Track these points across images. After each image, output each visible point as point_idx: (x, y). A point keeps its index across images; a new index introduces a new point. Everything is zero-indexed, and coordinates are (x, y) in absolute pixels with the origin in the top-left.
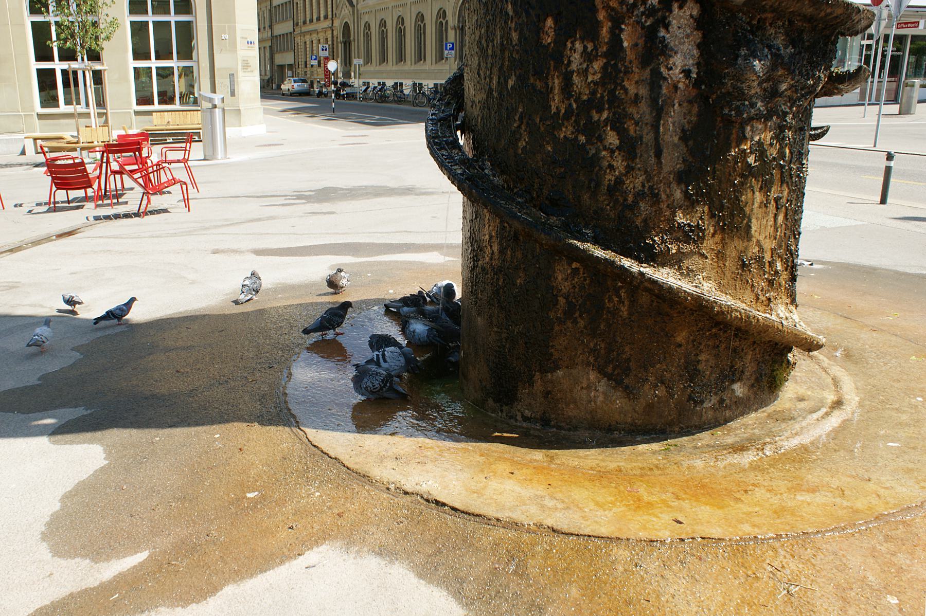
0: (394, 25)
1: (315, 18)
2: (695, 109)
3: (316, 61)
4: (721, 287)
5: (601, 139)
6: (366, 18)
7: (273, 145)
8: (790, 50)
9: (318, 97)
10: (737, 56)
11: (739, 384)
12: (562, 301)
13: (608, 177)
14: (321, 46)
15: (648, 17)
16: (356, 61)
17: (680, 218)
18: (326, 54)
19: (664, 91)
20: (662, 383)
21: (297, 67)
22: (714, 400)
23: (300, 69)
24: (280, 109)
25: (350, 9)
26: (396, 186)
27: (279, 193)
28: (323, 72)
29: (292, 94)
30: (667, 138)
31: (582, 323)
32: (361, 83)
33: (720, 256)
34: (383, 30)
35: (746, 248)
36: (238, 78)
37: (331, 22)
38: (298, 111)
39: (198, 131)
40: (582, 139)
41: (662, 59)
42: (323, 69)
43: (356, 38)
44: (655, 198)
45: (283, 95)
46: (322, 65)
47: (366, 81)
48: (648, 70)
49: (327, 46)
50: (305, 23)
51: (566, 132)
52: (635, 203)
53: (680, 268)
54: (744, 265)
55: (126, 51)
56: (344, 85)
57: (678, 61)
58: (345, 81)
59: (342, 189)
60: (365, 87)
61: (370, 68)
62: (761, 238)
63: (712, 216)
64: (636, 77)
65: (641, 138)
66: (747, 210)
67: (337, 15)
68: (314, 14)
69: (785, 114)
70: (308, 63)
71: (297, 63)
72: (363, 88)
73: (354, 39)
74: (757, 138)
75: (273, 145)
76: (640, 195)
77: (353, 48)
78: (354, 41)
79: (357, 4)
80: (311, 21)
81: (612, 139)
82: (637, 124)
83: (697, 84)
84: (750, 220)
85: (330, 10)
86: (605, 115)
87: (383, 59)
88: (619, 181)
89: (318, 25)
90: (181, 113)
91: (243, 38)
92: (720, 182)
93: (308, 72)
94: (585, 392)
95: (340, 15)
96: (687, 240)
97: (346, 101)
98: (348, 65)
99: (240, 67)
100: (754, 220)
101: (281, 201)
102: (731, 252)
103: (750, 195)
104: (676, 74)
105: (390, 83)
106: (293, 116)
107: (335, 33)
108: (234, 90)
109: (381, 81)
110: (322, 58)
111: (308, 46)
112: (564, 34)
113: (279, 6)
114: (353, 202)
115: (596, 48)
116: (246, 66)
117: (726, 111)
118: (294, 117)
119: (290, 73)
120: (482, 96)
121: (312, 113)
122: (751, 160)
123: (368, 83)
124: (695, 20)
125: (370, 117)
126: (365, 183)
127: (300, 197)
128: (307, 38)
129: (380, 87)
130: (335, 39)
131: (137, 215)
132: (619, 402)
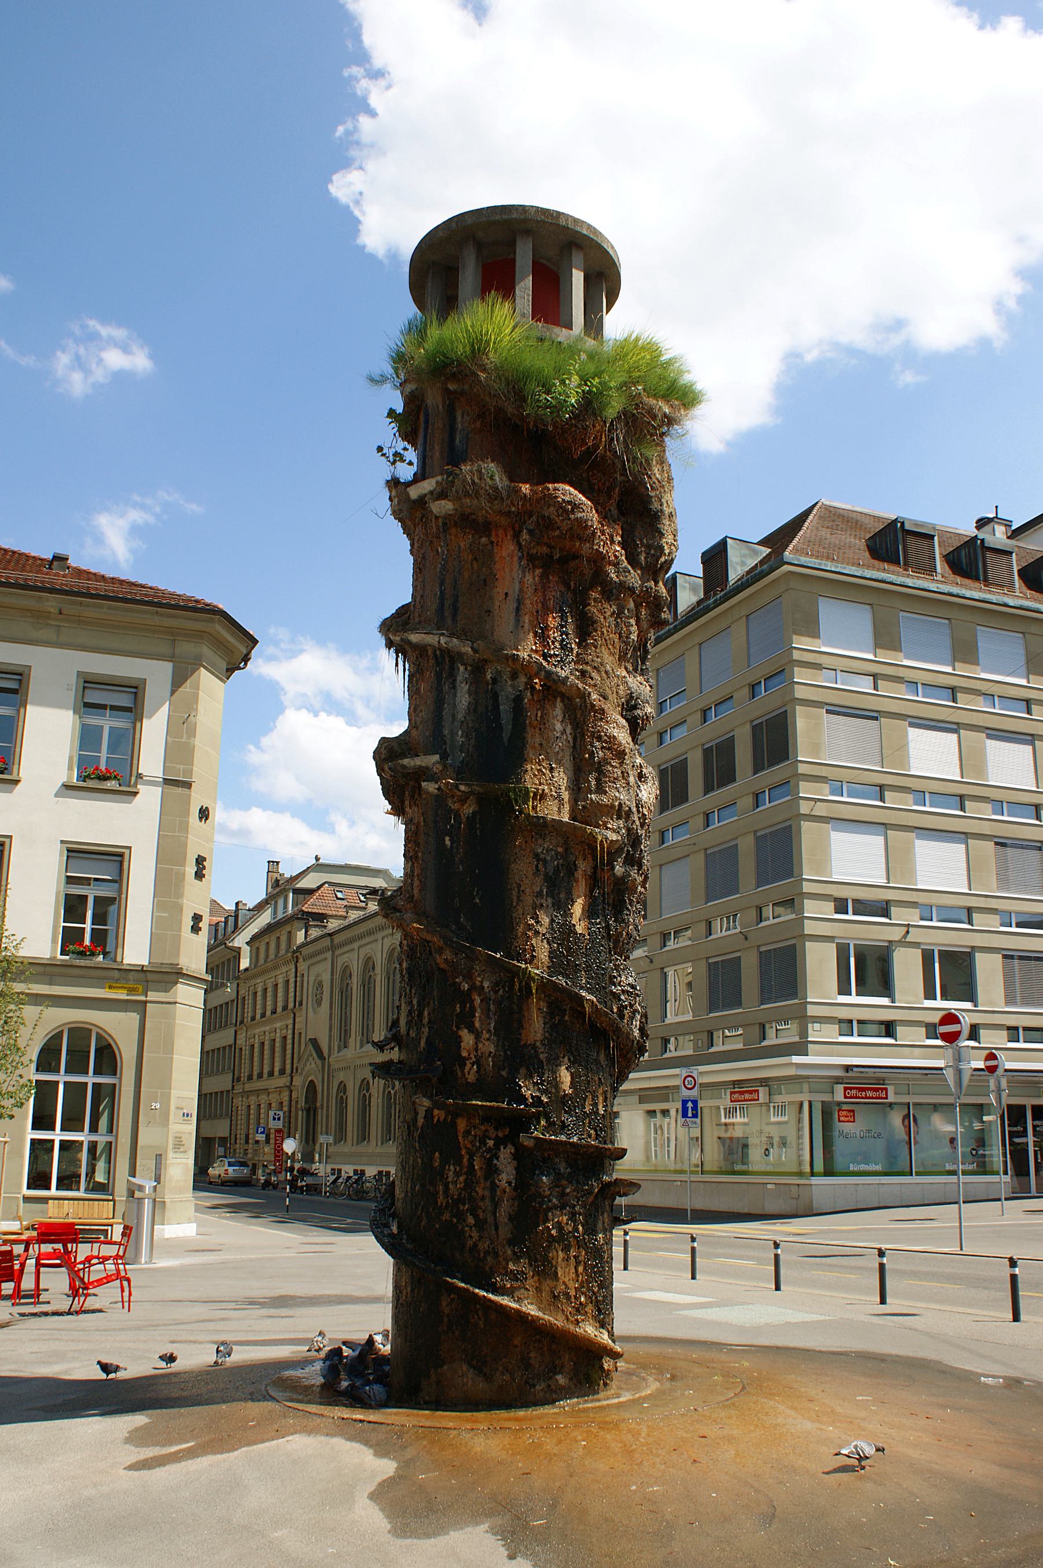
0: (381, 1088)
1: (266, 1071)
2: (516, 1204)
3: (264, 1135)
4: (540, 1309)
5: (465, 1221)
6: (341, 1076)
7: (208, 1250)
8: (569, 1170)
9: (264, 1189)
10: (534, 1174)
11: (560, 1376)
12: (446, 1319)
13: (469, 1242)
14: (271, 1113)
15: (488, 1153)
16: (322, 1139)
17: (511, 1266)
18: (279, 1125)
19: (498, 1193)
20: (507, 1371)
21: (233, 1141)
22: (543, 1385)
23: (238, 1146)
24: (208, 1204)
25: (319, 1062)
26: (364, 1295)
27: (227, 1299)
28: (273, 1151)
29: (224, 1183)
30: (501, 1219)
31: (457, 1333)
32: (329, 1171)
33: (539, 1290)
34: (364, 1094)
35: (556, 1286)
36: (166, 1159)
37: (289, 1078)
38: (235, 1208)
39: (106, 1228)
40: (455, 1220)
41: (495, 1175)
42: (272, 1146)
43: (325, 1105)
44: (496, 1255)
45: (211, 1183)
46: (272, 1141)
47: (337, 1167)
48: (489, 1182)
49: (281, 1113)
50: (250, 1078)
51: (446, 1216)
52: (485, 1258)
53: (513, 1297)
54: (554, 1297)
55: (26, 1118)
56: (303, 1172)
57: (504, 1177)
58: (306, 1166)
59: (301, 1297)
60: (334, 1177)
61: (346, 1148)
62: (566, 1280)
63: (531, 1265)
64: (483, 1186)
65: (486, 1219)
66: (554, 1263)
67: (299, 1070)
68: (265, 1066)
69: (574, 1206)
70: (251, 1136)
71: (233, 1137)
72: (332, 1178)
73: (322, 1105)
74: (556, 1220)
75: (208, 1250)
76: (487, 1253)
77: (320, 1119)
78: (322, 1108)
79: (329, 1056)
80: (260, 1076)
81: (471, 1220)
82: (484, 1211)
83: (515, 1189)
84: (556, 1268)
85: (288, 1062)
86: (467, 1206)
87: (363, 1136)
88: (475, 1245)
89: (270, 1082)
90: (87, 1202)
91: (178, 1108)
92: (534, 1245)
93: (250, 1151)
94: (460, 1379)
95: (303, 1069)
96: (517, 1280)
97: (305, 1196)
98: (311, 1142)
99: (170, 1146)
100: (559, 1269)
101: (233, 1305)
102: (546, 1287)
103: (555, 1253)
104: (503, 1184)
105: (371, 1171)
106: (228, 1215)
107: (294, 1095)
108: (160, 1176)
109: (359, 1168)
110: (272, 1131)
111: (252, 1112)
112: (445, 1161)
113: (213, 1051)
114: (314, 1308)
115: (461, 1170)
116: (179, 1145)
117: (534, 1204)
118: (230, 1217)
119: (221, 1151)
120: (403, 1195)
121: (257, 1212)
122: (554, 1232)
123: (340, 1170)
124: (513, 1155)
125: (338, 1220)
126: (328, 1292)
127: (252, 1302)
128: (253, 1100)
129: (356, 1177)
130: (293, 1103)
131: (69, 1313)
132: (482, 1385)
